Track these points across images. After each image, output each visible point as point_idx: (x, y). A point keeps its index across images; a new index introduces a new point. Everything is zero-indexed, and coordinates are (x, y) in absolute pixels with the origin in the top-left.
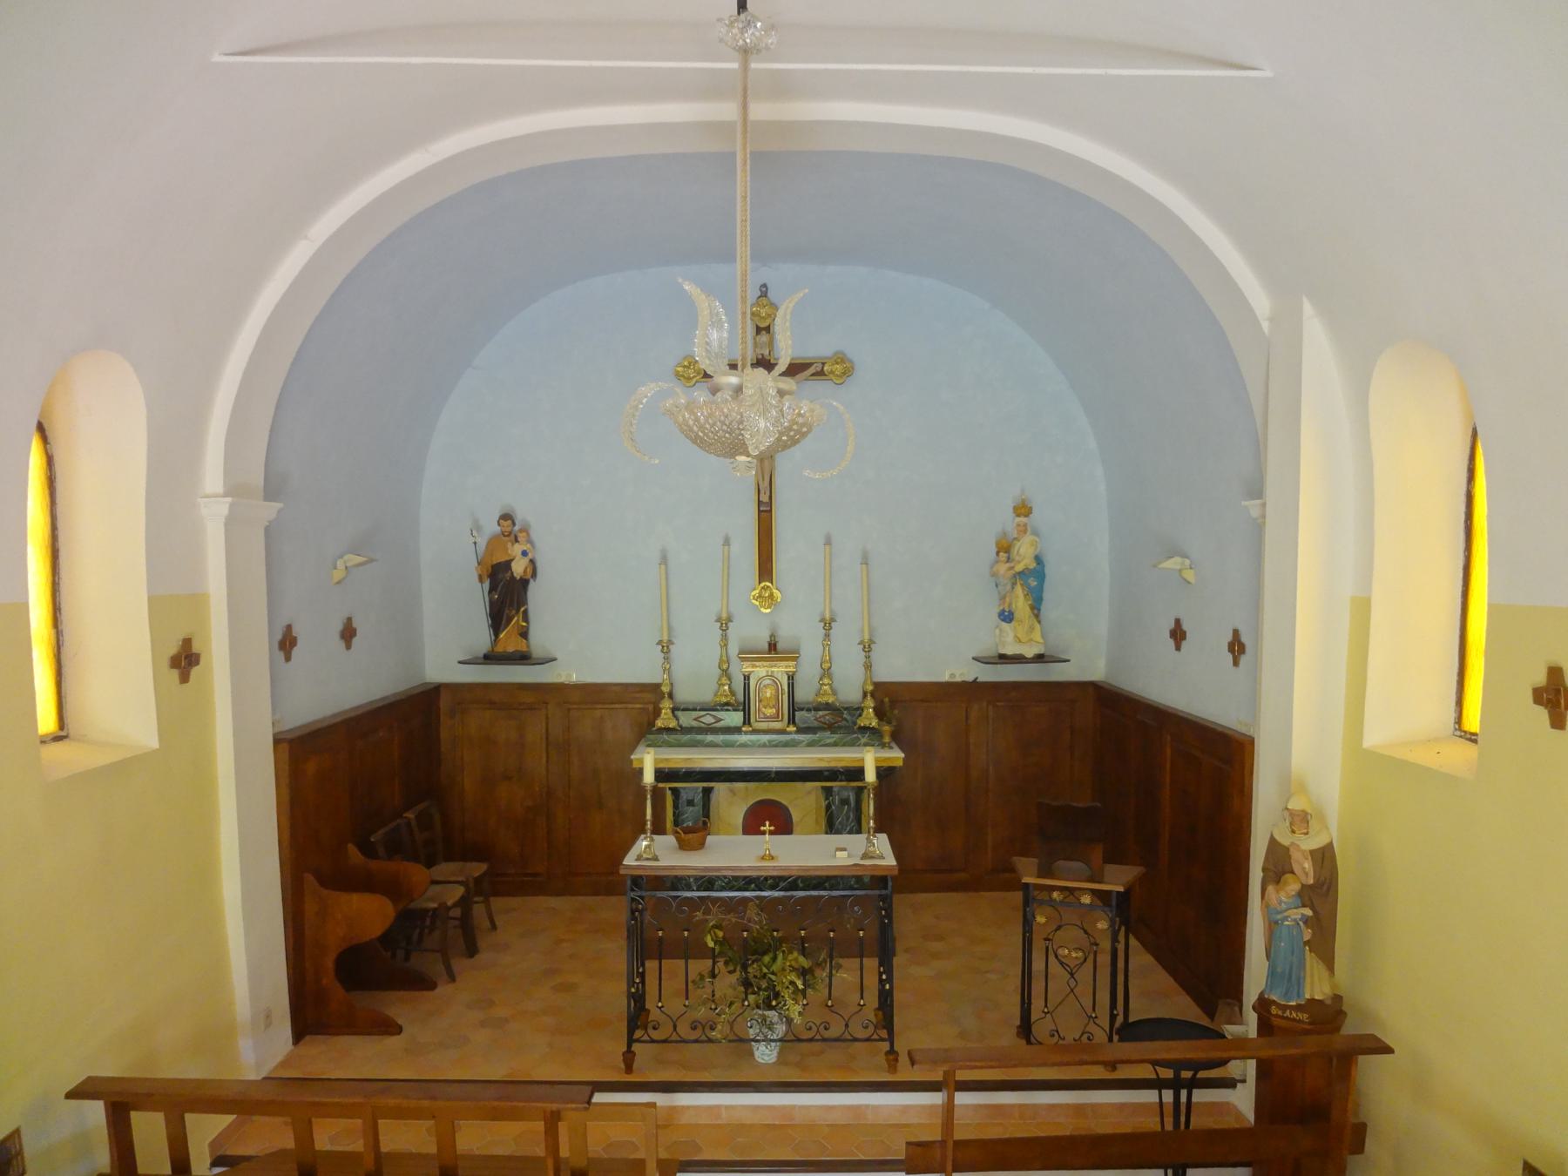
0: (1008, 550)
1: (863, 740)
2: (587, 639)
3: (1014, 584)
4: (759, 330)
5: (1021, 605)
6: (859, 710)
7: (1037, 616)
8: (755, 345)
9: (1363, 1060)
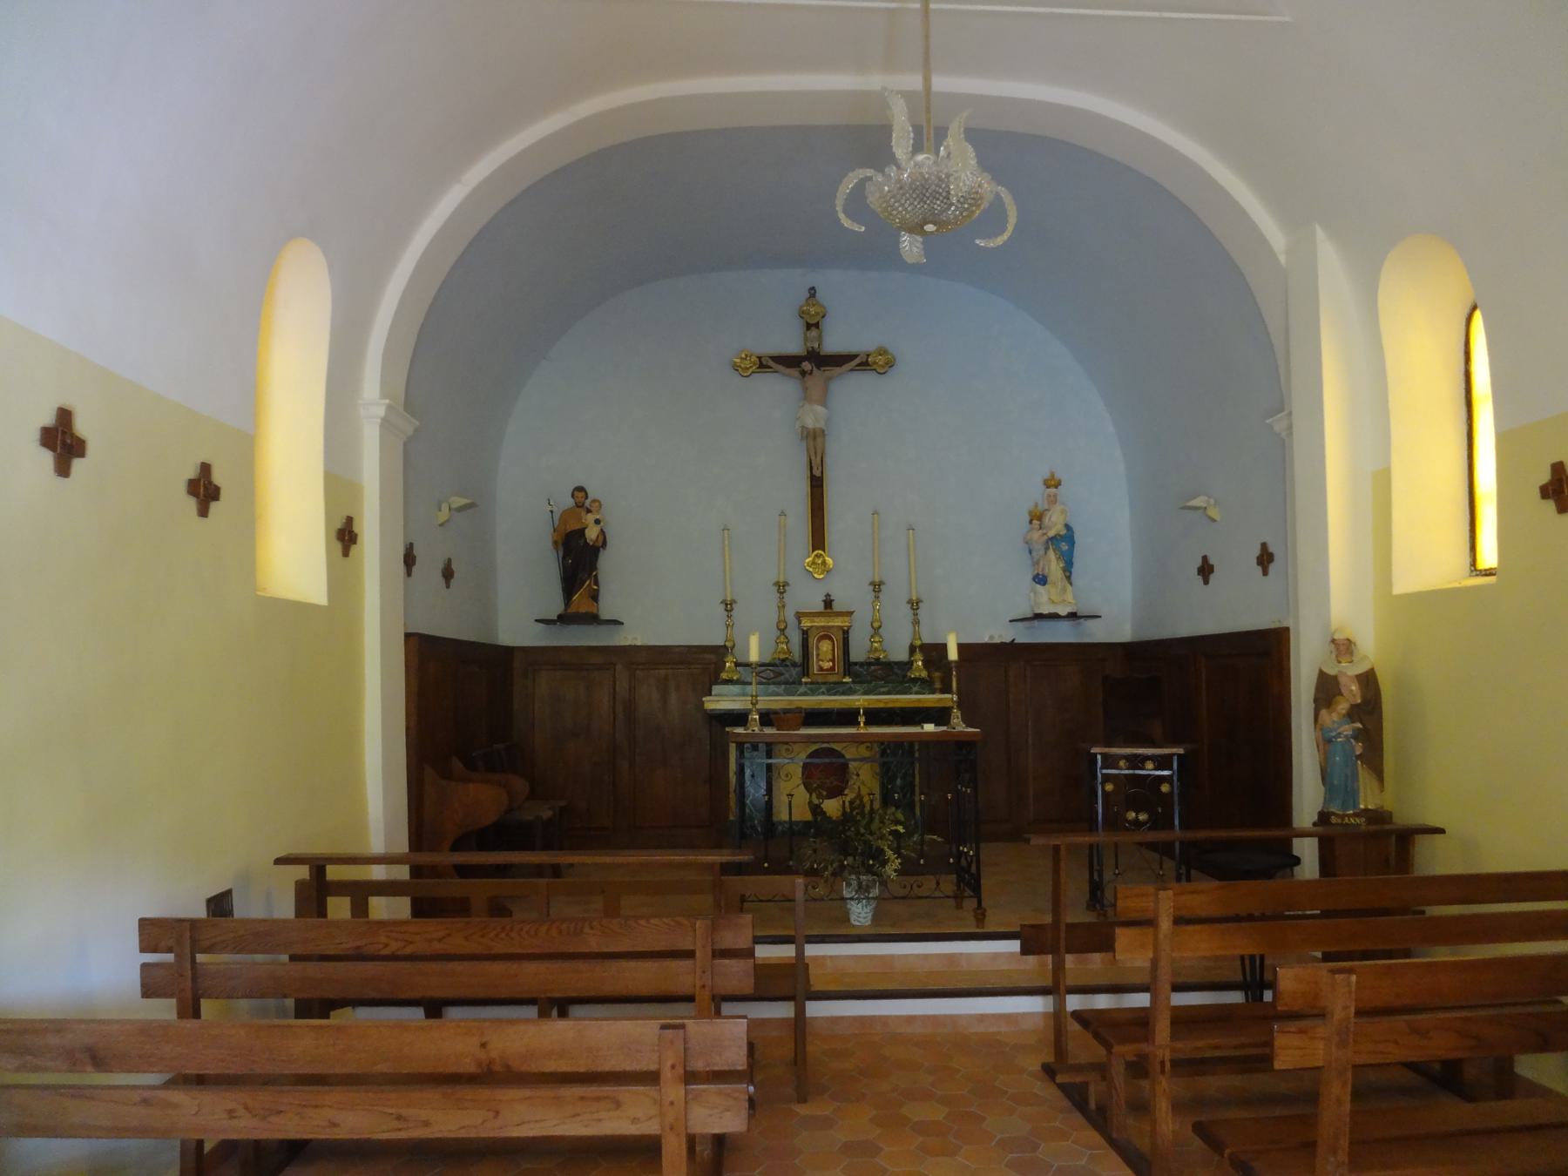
0: (1040, 518)
1: (915, 689)
2: (650, 607)
3: (1047, 549)
4: (809, 326)
5: (1054, 568)
6: (910, 664)
7: (1069, 578)
8: (806, 339)
9: (1419, 838)
